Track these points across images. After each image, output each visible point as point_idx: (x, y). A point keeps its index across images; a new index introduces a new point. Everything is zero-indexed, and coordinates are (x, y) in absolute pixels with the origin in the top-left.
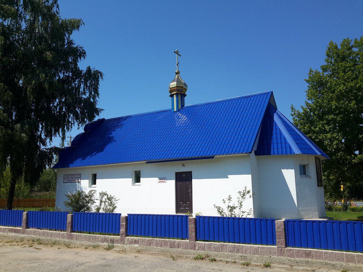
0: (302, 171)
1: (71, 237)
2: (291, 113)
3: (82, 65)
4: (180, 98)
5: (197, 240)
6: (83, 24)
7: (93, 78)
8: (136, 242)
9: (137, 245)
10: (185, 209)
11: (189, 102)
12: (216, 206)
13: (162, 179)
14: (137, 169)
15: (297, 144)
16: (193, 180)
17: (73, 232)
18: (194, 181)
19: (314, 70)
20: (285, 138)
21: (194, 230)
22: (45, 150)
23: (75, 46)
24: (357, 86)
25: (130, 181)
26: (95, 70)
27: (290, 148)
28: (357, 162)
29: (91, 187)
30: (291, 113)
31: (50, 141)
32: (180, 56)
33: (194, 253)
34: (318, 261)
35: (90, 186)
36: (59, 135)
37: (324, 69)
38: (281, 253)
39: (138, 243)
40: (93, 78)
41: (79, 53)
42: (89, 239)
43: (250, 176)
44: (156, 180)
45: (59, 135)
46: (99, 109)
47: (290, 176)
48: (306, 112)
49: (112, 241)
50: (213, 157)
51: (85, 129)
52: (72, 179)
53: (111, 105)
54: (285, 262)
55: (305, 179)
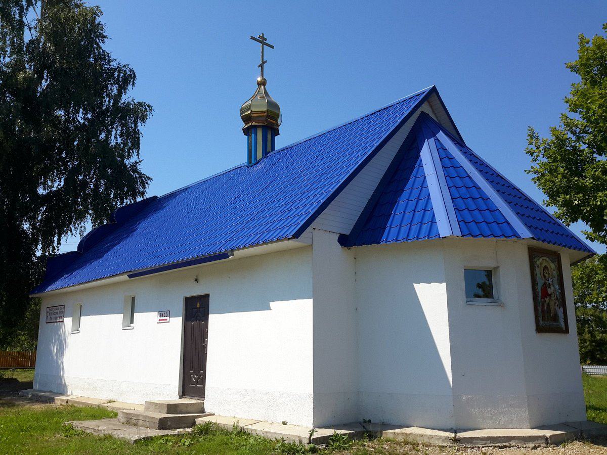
0: (480, 287)
2: (527, 148)
3: (131, 96)
4: (261, 135)
10: (196, 387)
11: (280, 143)
14: (132, 294)
15: (457, 209)
16: (211, 317)
18: (212, 318)
19: (591, 37)
20: (429, 197)
23: (114, 64)
26: (136, 102)
27: (433, 221)
29: (129, 328)
35: (74, 329)
40: (139, 112)
41: (127, 79)
44: (155, 315)
47: (434, 299)
48: (561, 142)
50: (225, 256)
55: (483, 310)
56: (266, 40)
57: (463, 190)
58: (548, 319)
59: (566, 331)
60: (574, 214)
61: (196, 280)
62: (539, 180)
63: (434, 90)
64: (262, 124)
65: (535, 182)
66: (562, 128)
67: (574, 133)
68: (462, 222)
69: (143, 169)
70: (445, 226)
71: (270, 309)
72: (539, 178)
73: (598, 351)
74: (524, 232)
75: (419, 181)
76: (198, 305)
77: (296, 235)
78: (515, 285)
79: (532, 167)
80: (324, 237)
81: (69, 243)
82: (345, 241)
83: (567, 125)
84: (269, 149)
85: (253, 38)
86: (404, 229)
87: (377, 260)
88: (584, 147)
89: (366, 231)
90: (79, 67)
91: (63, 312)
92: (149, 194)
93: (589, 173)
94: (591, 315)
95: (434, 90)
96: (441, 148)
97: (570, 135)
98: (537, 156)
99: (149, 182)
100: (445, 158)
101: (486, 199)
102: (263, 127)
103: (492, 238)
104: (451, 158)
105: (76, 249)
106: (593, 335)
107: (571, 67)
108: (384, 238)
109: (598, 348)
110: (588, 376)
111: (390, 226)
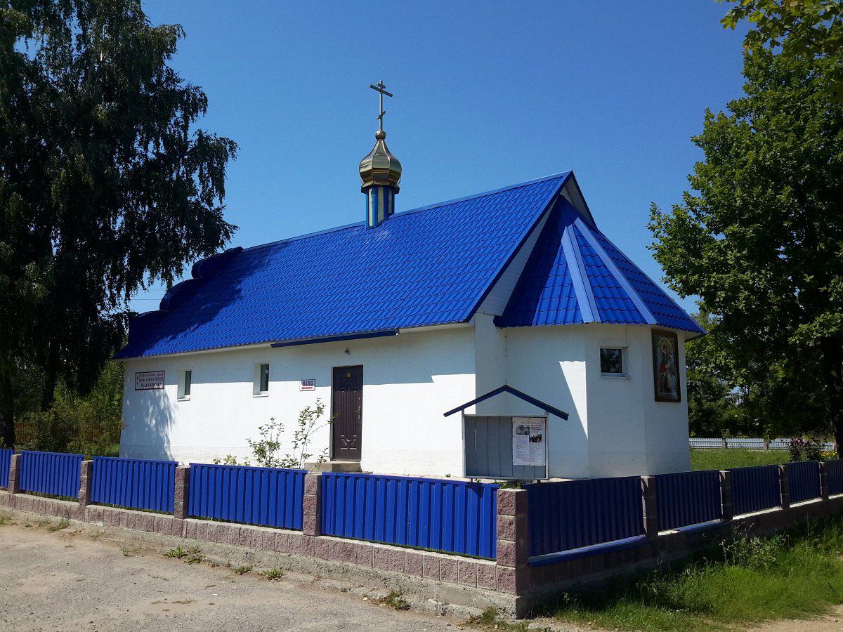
0: (610, 362)
1: (13, 503)
2: (649, 224)
3: (204, 125)
5: (186, 515)
6: (182, 36)
7: (213, 154)
8: (99, 516)
9: (100, 524)
11: (402, 204)
12: (252, 442)
13: (308, 383)
14: (264, 362)
15: (596, 297)
17: (20, 493)
18: (368, 390)
20: (572, 285)
21: (182, 493)
22: (106, 318)
23: (181, 86)
24: (802, 149)
25: (248, 387)
26: (218, 137)
27: (577, 307)
28: (798, 342)
30: (649, 224)
31: (126, 300)
32: (391, 95)
33: (177, 541)
34: (363, 568)
36: (143, 286)
37: (739, 110)
38: (308, 547)
39: (102, 520)
40: (213, 154)
41: (194, 103)
42: (36, 507)
43: (473, 376)
44: (299, 384)
45: (143, 286)
46: (228, 225)
47: (575, 374)
48: (681, 221)
49: (68, 513)
50: (392, 333)
51: (194, 272)
52: (149, 382)
53: (253, 213)
54: (311, 569)
55: (613, 383)
56: (384, 87)
57: (600, 279)
58: (664, 392)
59: (679, 400)
60: (688, 289)
61: (347, 351)
62: (659, 256)
63: (571, 175)
64: (383, 182)
65: (655, 259)
66: (683, 205)
67: (694, 211)
68: (601, 309)
69: (227, 217)
70: (587, 313)
71: (431, 381)
72: (660, 255)
73: (705, 421)
74: (651, 320)
75: (562, 268)
76: (349, 375)
77: (467, 320)
78: (639, 362)
79: (653, 244)
80: (484, 321)
81: (147, 297)
82: (499, 322)
83: (689, 203)
84: (390, 211)
85: (372, 87)
86: (552, 314)
87: (529, 342)
88: (703, 226)
89: (518, 313)
90: (139, 86)
91: (163, 379)
92: (230, 245)
93: (705, 255)
94: (699, 380)
95: (571, 175)
96: (579, 236)
97: (691, 214)
98: (658, 233)
99: (234, 231)
100: (583, 245)
101: (618, 287)
102: (385, 187)
103: (625, 325)
104: (587, 245)
105: (158, 309)
106: (700, 404)
107: (697, 141)
108: (534, 321)
109: (704, 419)
110: (692, 449)
111: (539, 311)
